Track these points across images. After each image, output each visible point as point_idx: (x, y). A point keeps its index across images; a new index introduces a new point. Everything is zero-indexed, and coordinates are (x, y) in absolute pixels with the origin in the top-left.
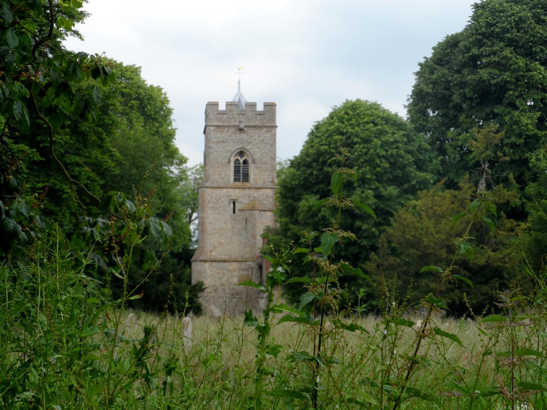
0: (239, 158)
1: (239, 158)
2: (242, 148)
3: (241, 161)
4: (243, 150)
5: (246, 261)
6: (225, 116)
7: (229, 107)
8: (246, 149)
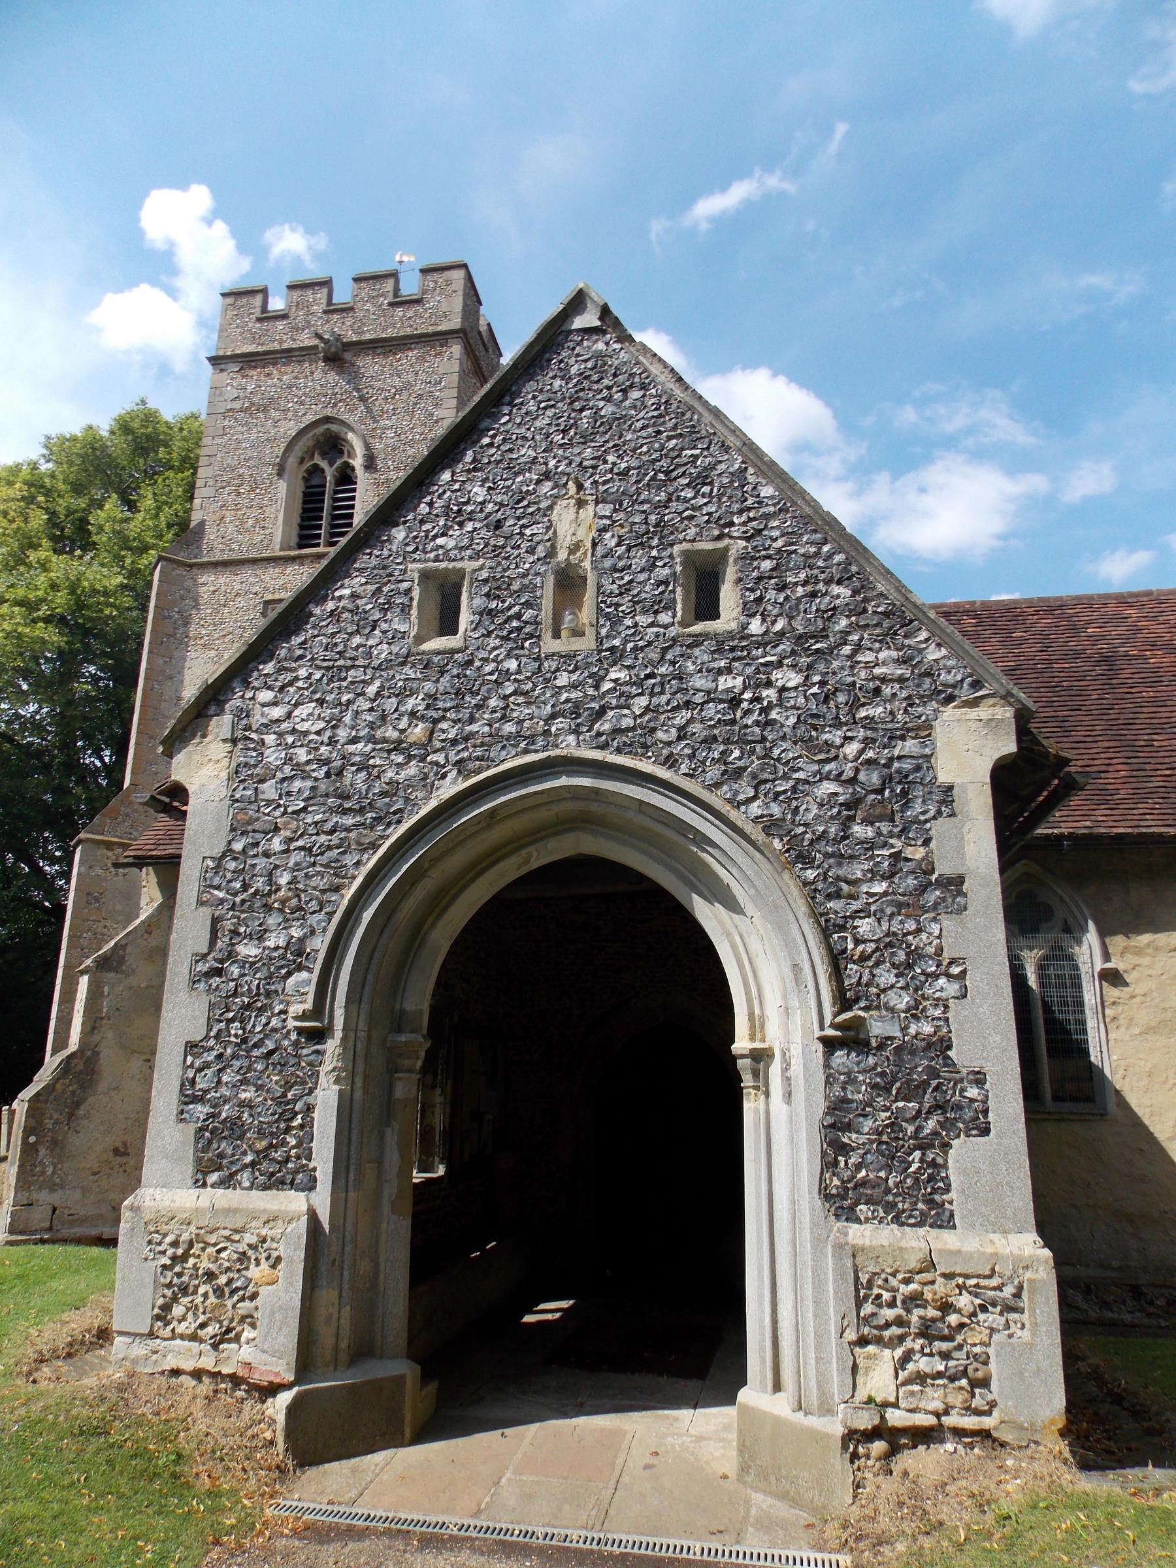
0: (324, 464)
1: (324, 464)
2: (327, 420)
3: (330, 473)
4: (334, 427)
6: (280, 325)
7: (296, 294)
8: (342, 423)
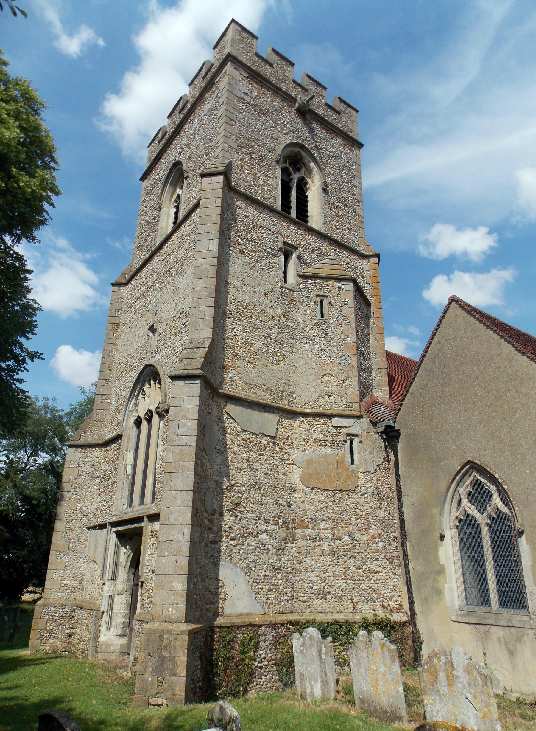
4: (303, 154)
5: (330, 416)
8: (312, 155)
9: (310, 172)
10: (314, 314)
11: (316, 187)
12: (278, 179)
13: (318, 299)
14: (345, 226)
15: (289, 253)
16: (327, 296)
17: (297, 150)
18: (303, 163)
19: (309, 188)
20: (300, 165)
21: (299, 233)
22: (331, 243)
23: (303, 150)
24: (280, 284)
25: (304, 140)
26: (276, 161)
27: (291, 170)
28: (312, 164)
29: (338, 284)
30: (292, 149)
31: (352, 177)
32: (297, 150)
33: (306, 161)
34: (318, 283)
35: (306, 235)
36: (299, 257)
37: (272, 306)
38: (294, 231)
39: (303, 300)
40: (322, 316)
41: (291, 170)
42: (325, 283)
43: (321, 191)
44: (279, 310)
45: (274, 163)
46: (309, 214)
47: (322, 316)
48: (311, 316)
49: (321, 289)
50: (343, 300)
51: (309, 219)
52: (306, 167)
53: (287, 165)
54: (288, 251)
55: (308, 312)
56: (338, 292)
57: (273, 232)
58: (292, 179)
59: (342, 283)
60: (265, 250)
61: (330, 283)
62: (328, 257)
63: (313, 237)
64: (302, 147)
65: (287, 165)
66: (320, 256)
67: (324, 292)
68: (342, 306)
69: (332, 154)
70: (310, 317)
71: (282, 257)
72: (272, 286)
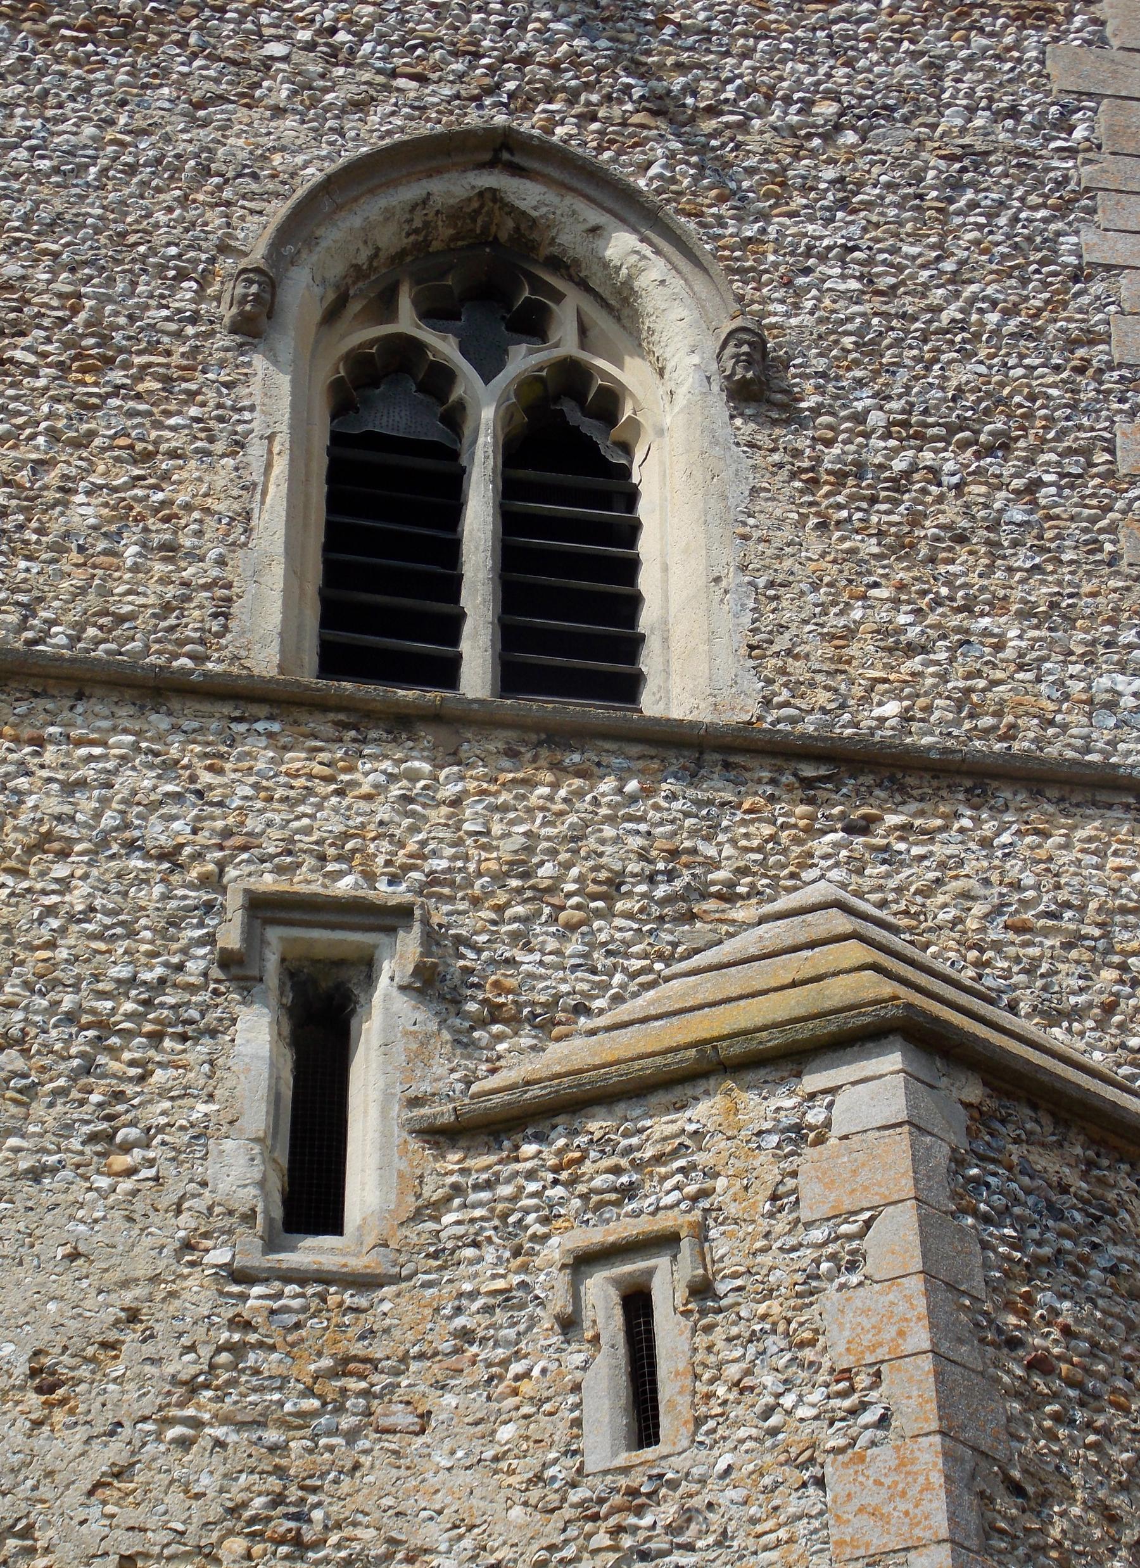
4: (527, 195)
9: (620, 304)
10: (562, 1433)
11: (681, 400)
12: (256, 450)
13: (600, 1293)
14: (998, 605)
15: (354, 977)
16: (667, 1241)
17: (455, 187)
18: (557, 264)
19: (634, 423)
20: (539, 285)
21: (449, 791)
22: (808, 783)
23: (517, 170)
24: (220, 1256)
25: (522, 102)
26: (234, 330)
27: (444, 346)
28: (622, 246)
29: (765, 1106)
30: (410, 193)
31: (1063, 209)
32: (455, 187)
33: (570, 239)
34: (603, 1144)
35: (530, 783)
36: (428, 983)
37: (120, 1473)
38: (395, 791)
39: (466, 1335)
40: (644, 1424)
41: (444, 346)
42: (662, 1126)
43: (720, 406)
44: (205, 1482)
45: (223, 340)
46: (647, 620)
47: (644, 1424)
48: (532, 1463)
49: (629, 1192)
50: (818, 1235)
51: (650, 662)
52: (583, 285)
53: (407, 321)
54: (341, 963)
55: (506, 1433)
56: (772, 1175)
57: (169, 855)
58: (461, 406)
59: (812, 1082)
60: (70, 1018)
61: (705, 1111)
62: (784, 902)
63: (607, 785)
64: (502, 150)
65: (407, 321)
66: (691, 917)
67: (662, 1203)
68: (809, 1288)
69: (826, 109)
70: (526, 1467)
71: (255, 1037)
72: (128, 1297)
